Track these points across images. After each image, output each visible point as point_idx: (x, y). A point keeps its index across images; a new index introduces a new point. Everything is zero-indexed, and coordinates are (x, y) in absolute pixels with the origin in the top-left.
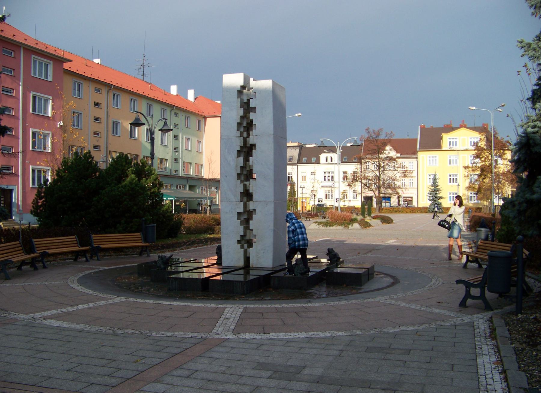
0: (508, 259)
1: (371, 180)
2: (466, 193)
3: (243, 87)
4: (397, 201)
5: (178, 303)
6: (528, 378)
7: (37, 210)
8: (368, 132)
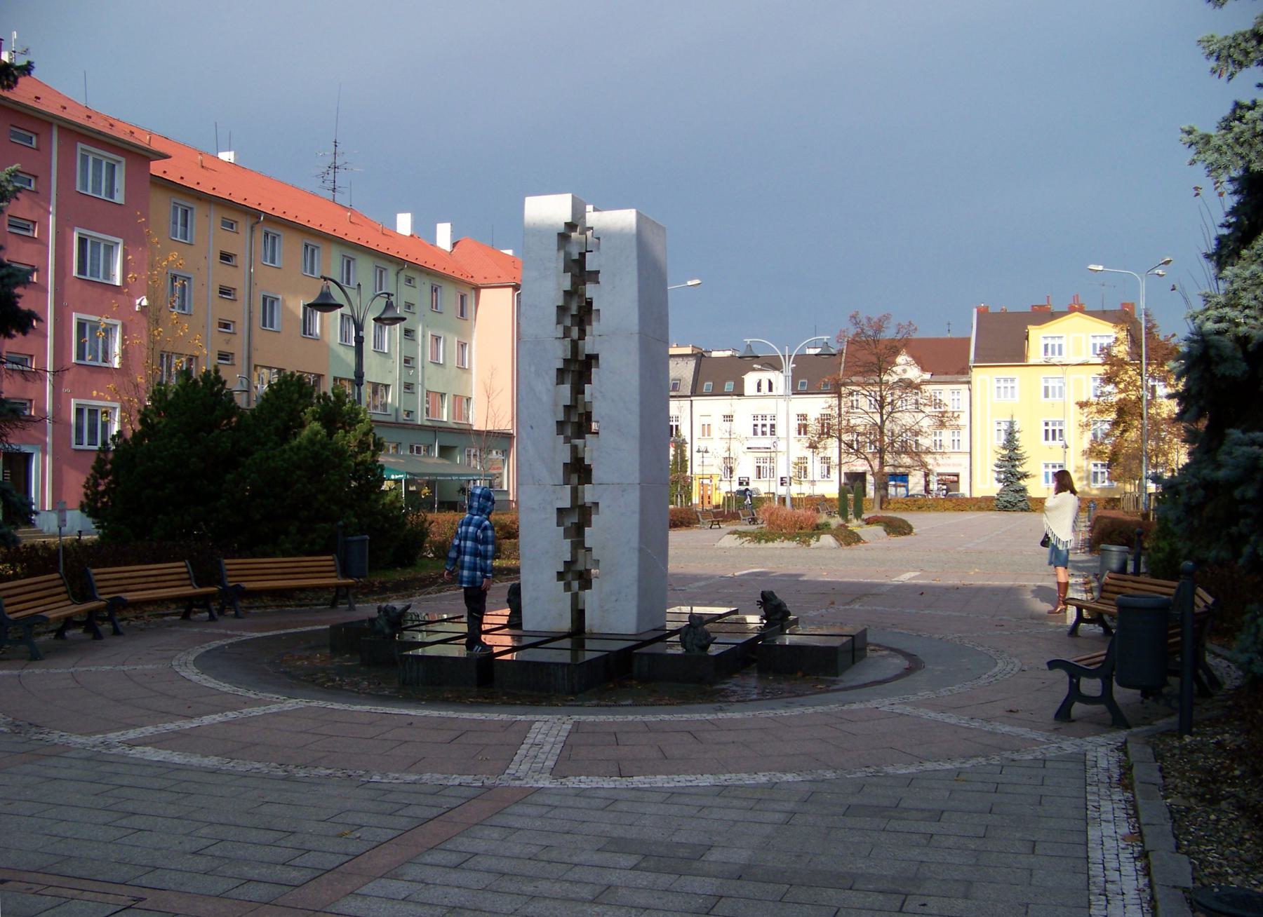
0: (1161, 612)
1: (864, 434)
2: (1084, 463)
3: (571, 226)
4: (923, 482)
5: (426, 712)
6: (1194, 869)
7: (96, 502)
8: (856, 323)
